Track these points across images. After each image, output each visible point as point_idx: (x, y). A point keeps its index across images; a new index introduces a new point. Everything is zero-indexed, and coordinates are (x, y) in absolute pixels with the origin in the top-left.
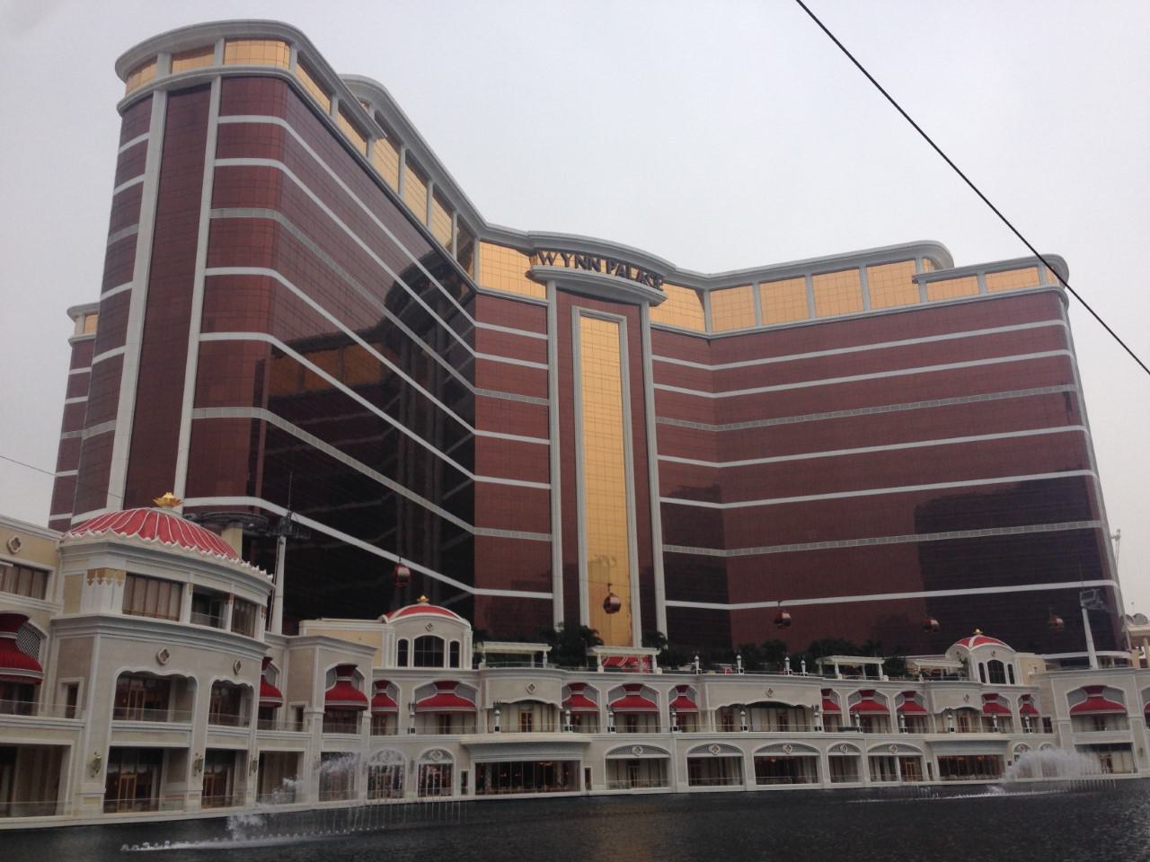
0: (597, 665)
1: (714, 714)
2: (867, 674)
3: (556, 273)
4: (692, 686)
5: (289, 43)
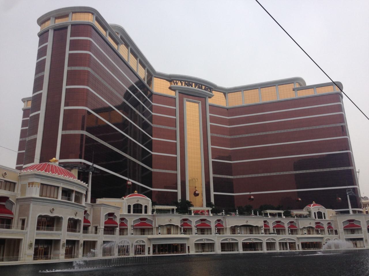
0: (191, 213)
1: (229, 229)
2: (278, 216)
3: (178, 87)
4: (222, 220)
5: (93, 14)
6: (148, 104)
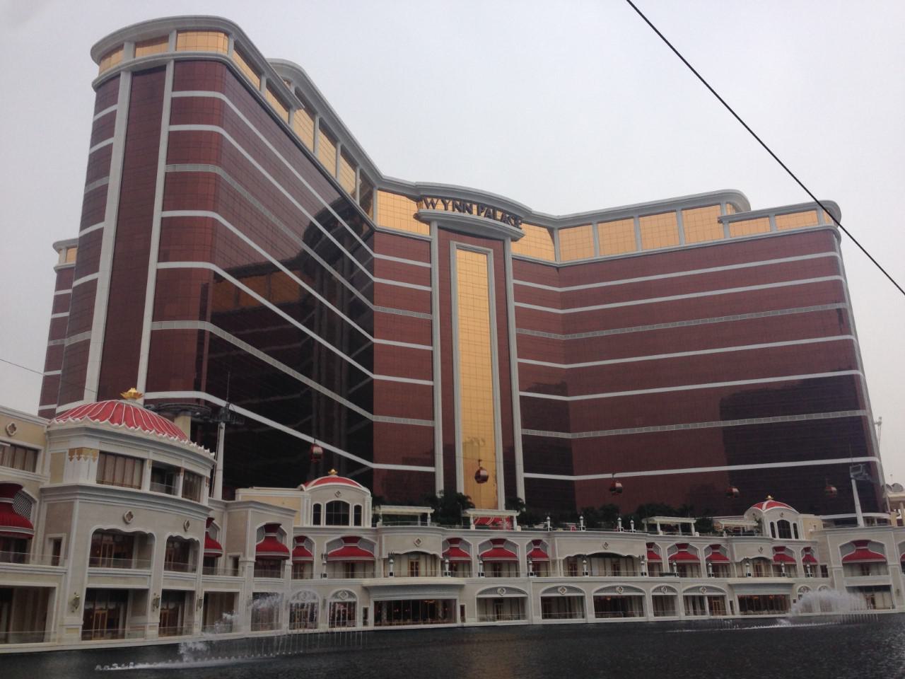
0: (469, 524)
1: (562, 562)
2: (683, 531)
3: (437, 215)
4: (544, 540)
5: (227, 34)
6: (364, 257)
